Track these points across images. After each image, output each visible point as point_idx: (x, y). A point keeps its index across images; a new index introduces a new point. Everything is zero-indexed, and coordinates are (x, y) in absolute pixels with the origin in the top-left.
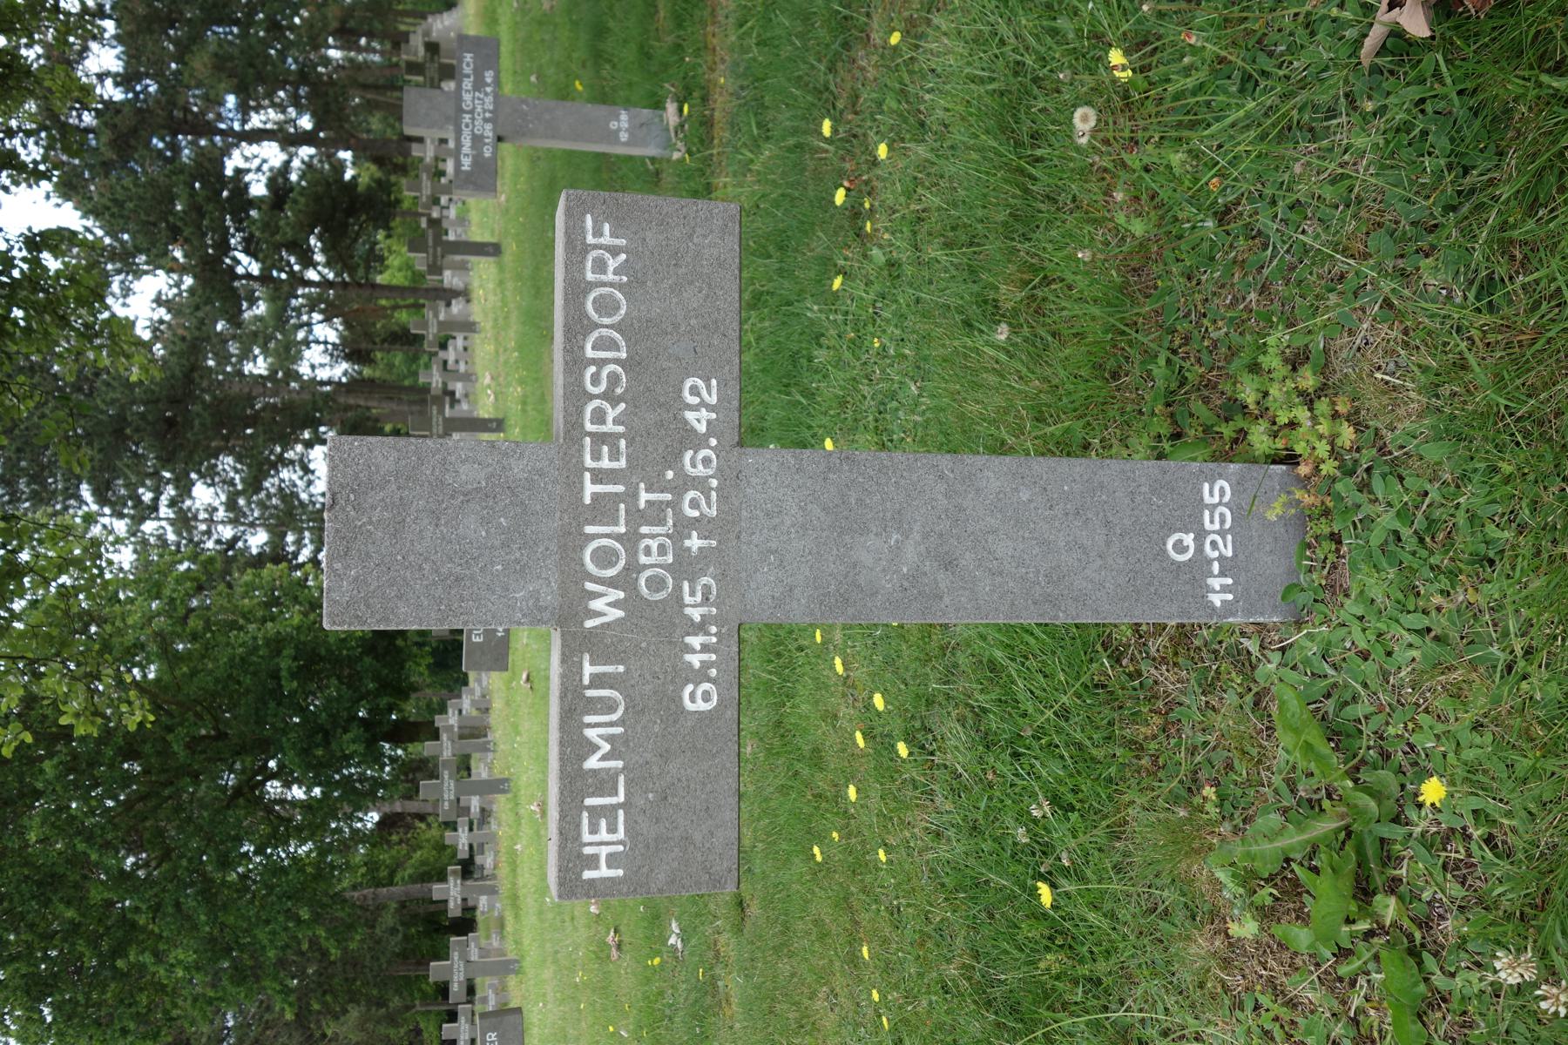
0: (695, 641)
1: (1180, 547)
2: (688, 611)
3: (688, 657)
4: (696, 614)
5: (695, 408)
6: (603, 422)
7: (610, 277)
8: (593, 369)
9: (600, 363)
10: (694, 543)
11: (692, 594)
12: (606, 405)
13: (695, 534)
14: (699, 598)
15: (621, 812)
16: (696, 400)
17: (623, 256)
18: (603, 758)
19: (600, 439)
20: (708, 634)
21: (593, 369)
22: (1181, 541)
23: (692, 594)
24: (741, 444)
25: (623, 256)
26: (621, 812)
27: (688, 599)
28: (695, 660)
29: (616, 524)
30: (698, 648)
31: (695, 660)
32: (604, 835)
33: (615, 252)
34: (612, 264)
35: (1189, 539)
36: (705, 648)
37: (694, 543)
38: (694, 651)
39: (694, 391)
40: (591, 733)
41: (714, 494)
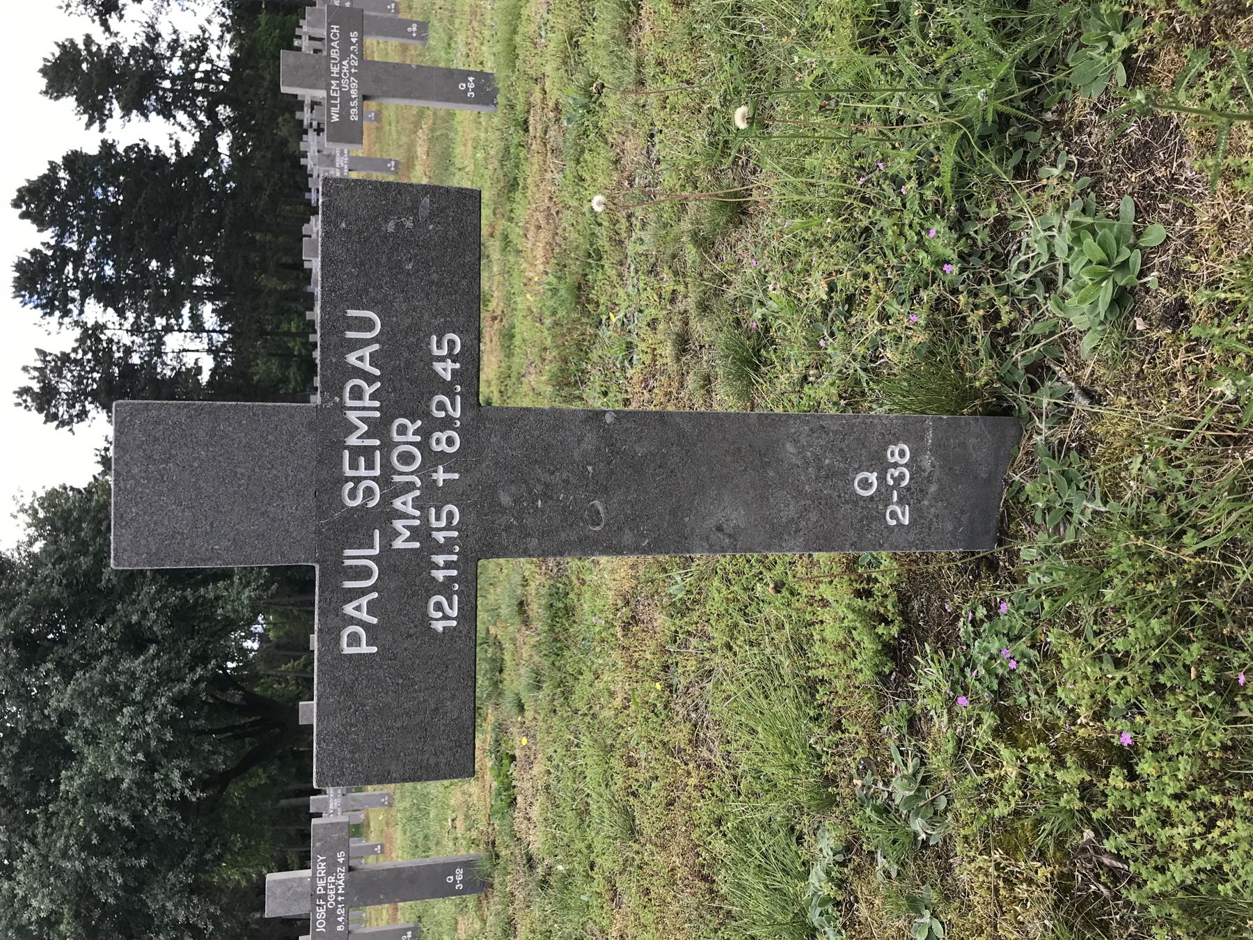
0: (440, 559)
1: (865, 484)
2: (434, 573)
3: (434, 573)
4: (440, 537)
5: (442, 359)
6: (360, 398)
7: (367, 402)
8: (351, 485)
9: (357, 480)
10: (441, 476)
11: (438, 518)
12: (363, 384)
13: (441, 468)
14: (443, 523)
15: (378, 453)
16: (440, 614)
17: (378, 384)
18: (405, 541)
19: (356, 452)
20: (451, 552)
21: (351, 485)
22: (867, 479)
23: (438, 518)
24: (495, 105)
25: (378, 384)
26: (378, 453)
27: (434, 524)
28: (440, 575)
29: (372, 547)
30: (442, 564)
31: (440, 575)
32: (362, 472)
33: (370, 379)
34: (368, 390)
35: (873, 477)
36: (448, 565)
37: (441, 476)
38: (438, 568)
39: (438, 607)
40: (352, 416)
41: (456, 598)
